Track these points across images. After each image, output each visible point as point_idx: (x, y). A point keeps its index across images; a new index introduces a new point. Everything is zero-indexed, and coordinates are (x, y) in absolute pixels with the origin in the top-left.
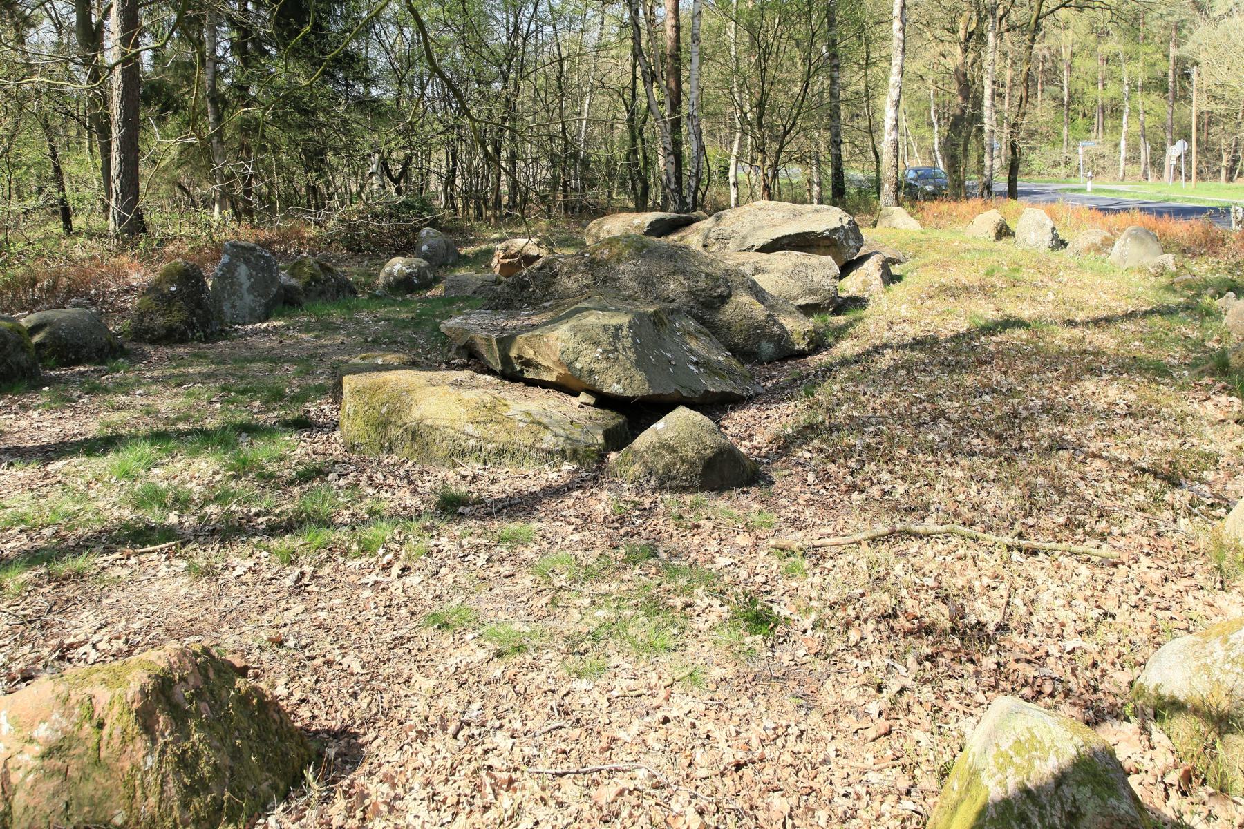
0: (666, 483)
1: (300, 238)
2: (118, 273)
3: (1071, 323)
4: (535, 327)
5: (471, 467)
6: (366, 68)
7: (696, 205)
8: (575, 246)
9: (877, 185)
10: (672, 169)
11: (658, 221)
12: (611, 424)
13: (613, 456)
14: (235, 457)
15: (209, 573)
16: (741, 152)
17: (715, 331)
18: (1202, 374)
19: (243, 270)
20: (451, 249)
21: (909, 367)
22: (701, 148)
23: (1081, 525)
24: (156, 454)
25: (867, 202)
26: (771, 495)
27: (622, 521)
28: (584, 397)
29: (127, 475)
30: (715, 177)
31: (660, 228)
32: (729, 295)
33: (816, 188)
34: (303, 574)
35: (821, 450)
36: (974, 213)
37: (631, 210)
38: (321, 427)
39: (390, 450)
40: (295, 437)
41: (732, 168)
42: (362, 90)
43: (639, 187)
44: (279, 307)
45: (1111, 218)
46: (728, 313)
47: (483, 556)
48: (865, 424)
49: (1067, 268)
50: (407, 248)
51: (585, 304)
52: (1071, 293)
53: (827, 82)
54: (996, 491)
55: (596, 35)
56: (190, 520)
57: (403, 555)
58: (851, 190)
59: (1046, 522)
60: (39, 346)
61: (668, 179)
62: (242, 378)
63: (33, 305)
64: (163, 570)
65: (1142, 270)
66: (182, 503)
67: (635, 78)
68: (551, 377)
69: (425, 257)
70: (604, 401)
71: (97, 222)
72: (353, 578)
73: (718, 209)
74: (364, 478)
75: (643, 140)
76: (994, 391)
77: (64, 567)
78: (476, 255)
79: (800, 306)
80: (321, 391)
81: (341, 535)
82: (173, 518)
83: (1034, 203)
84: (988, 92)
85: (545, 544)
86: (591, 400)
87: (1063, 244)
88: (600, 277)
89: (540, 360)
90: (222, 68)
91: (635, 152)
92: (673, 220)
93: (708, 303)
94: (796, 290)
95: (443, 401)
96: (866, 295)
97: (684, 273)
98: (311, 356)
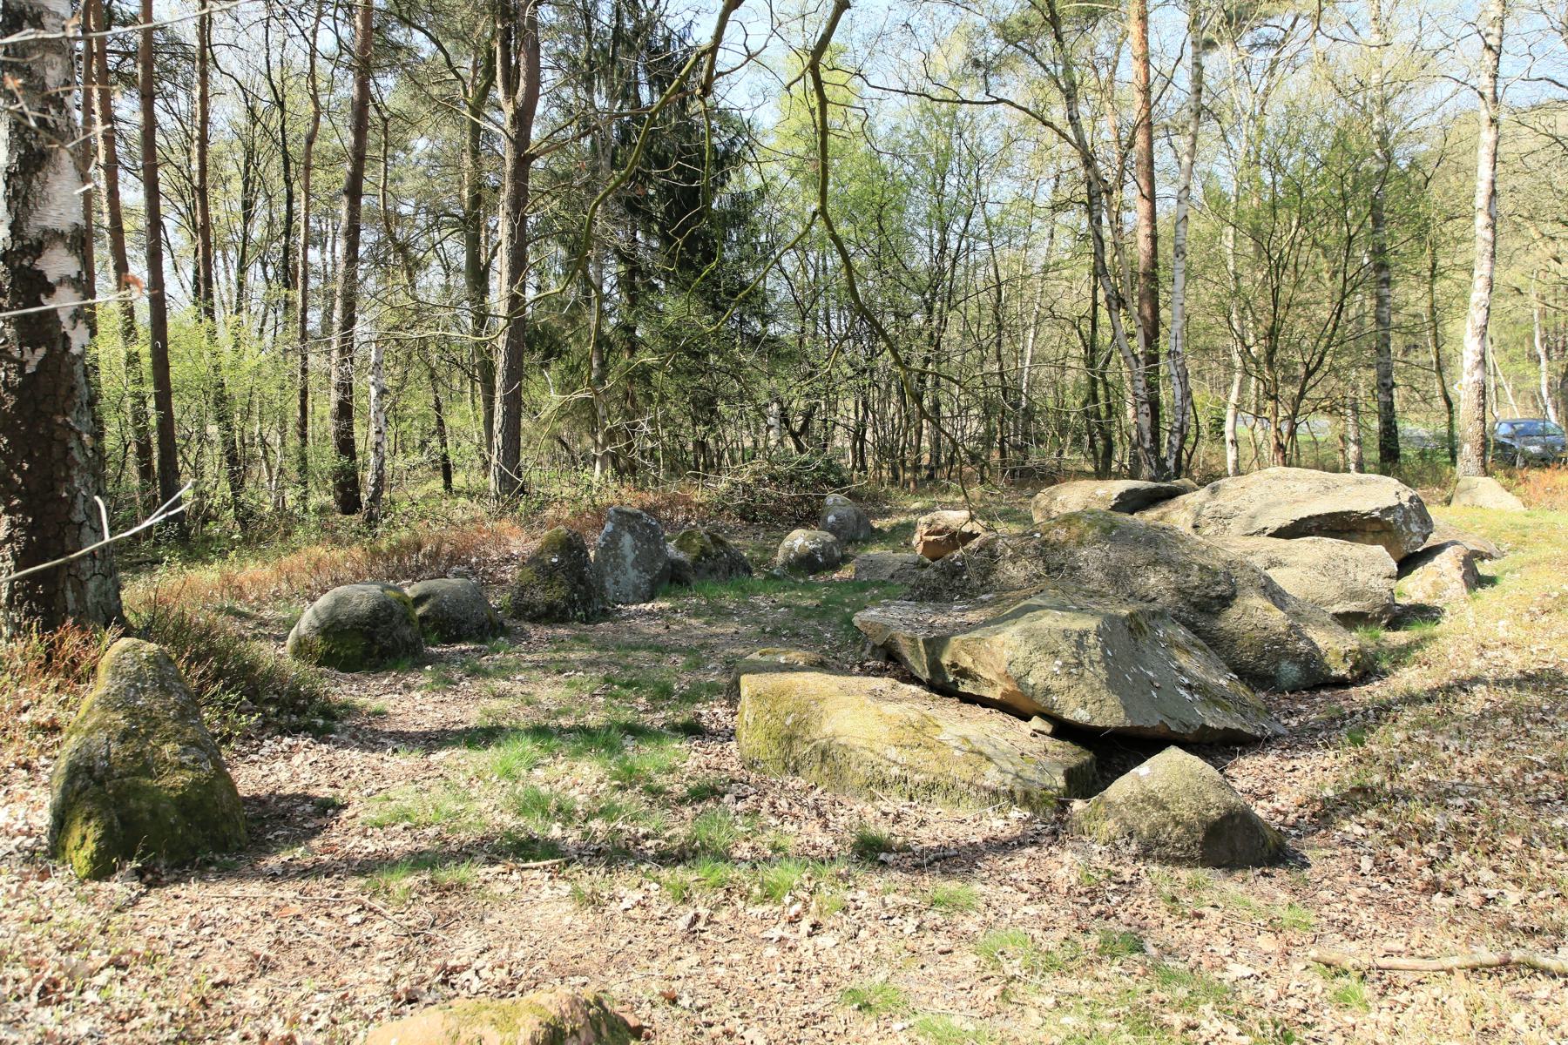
1: (687, 502)
2: (499, 539)
4: (970, 627)
5: (894, 802)
6: (765, 300)
8: (1018, 521)
10: (1146, 422)
11: (1129, 492)
13: (1078, 805)
14: (621, 763)
15: (593, 901)
17: (1215, 643)
20: (862, 520)
22: (1187, 394)
25: (1436, 470)
27: (1093, 895)
28: (1037, 723)
30: (1204, 432)
31: (1133, 502)
32: (1233, 596)
33: (1353, 448)
34: (697, 917)
37: (1087, 475)
38: (714, 735)
39: (796, 772)
40: (685, 745)
41: (1229, 419)
42: (759, 327)
43: (1100, 444)
44: (666, 586)
47: (911, 922)
50: (810, 517)
53: (1370, 303)
55: (1043, 251)
57: (813, 907)
58: (1408, 451)
60: (423, 619)
61: (1141, 435)
62: (626, 668)
63: (416, 573)
64: (547, 893)
66: (565, 813)
67: (1095, 305)
68: (995, 694)
69: (832, 530)
70: (1064, 730)
71: (476, 480)
72: (754, 929)
73: (1210, 478)
74: (765, 804)
75: (1106, 384)
77: (448, 875)
78: (894, 529)
79: (1336, 615)
80: (714, 690)
81: (740, 873)
82: (556, 831)
86: (1048, 728)
88: (1054, 564)
89: (980, 670)
90: (607, 306)
91: (1095, 399)
92: (1150, 491)
95: (861, 715)
98: (702, 646)
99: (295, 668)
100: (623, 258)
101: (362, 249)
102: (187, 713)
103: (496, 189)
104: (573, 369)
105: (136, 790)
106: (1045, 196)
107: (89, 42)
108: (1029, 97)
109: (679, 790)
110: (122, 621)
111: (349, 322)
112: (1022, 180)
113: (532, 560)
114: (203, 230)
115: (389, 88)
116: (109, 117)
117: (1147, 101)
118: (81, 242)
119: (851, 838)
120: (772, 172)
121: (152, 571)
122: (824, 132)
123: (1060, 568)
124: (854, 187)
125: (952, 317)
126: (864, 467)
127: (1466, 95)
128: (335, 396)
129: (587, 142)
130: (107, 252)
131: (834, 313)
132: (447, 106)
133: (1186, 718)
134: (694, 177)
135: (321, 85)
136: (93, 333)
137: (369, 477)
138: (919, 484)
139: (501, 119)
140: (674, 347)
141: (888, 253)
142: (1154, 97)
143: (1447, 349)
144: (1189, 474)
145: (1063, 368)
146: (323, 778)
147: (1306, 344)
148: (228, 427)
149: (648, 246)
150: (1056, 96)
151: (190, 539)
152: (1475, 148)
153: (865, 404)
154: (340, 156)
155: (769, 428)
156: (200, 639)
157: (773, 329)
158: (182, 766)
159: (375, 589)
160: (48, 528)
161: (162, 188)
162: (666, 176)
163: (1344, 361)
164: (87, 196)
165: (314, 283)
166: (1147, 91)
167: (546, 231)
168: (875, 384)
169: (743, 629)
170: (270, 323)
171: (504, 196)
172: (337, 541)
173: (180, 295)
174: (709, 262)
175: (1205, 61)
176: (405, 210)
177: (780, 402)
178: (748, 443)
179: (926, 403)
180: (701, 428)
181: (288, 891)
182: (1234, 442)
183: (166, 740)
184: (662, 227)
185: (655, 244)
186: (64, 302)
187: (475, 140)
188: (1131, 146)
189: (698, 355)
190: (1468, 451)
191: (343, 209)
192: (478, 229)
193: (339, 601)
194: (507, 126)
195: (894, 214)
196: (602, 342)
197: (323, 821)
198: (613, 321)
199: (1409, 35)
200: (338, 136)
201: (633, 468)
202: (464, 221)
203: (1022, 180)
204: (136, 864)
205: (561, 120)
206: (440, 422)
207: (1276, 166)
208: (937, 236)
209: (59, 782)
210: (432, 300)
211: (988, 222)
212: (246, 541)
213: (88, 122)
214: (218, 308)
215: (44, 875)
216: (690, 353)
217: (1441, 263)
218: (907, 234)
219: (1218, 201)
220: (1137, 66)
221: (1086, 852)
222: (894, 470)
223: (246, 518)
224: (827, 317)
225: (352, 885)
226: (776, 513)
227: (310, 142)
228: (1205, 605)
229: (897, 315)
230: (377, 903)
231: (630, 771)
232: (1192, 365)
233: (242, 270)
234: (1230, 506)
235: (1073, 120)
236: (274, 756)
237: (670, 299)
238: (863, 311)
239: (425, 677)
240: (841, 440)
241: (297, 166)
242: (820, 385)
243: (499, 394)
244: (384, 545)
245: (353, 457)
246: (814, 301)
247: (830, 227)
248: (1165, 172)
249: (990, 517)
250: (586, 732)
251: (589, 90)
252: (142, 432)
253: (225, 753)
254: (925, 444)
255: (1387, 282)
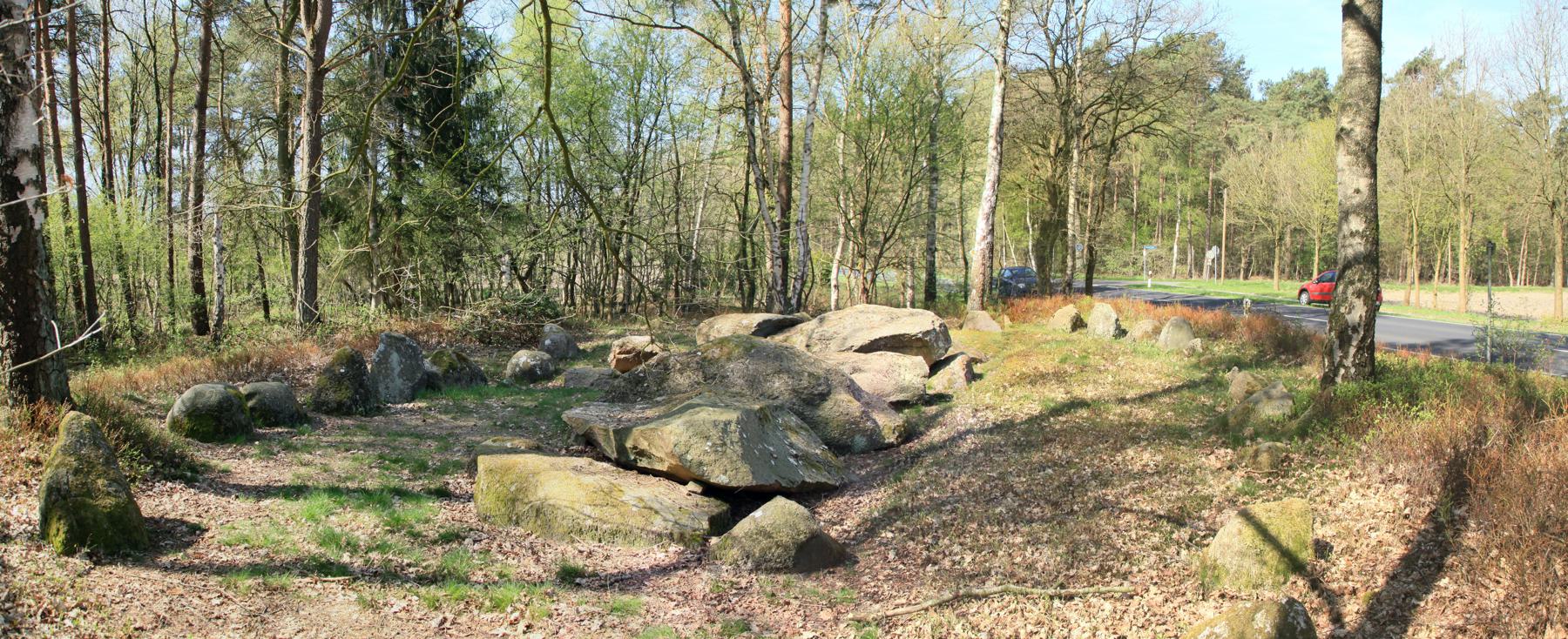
0: (761, 565)
1: (439, 329)
2: (302, 354)
3: (1123, 401)
4: (648, 420)
5: (587, 544)
6: (500, 176)
7: (800, 306)
8: (686, 343)
9: (965, 290)
10: (779, 271)
11: (765, 322)
12: (716, 511)
13: (714, 540)
14: (391, 515)
15: (372, 605)
16: (843, 257)
17: (814, 425)
18: (1210, 434)
19: (395, 357)
20: (571, 344)
21: (986, 449)
22: (808, 252)
23: (1110, 569)
24: (332, 505)
25: (956, 306)
26: (855, 573)
27: (720, 598)
28: (692, 486)
29: (312, 517)
30: (818, 280)
31: (767, 329)
32: (829, 393)
33: (910, 291)
34: (445, 620)
35: (902, 530)
36: (1055, 308)
37: (736, 310)
38: (458, 497)
39: (517, 523)
40: (437, 504)
41: (834, 270)
42: (496, 197)
43: (746, 287)
44: (423, 391)
45: (1160, 310)
46: (828, 409)
47: (597, 622)
48: (943, 504)
49: (1124, 353)
50: (532, 341)
51: (696, 401)
52: (1126, 375)
53: (926, 193)
54: (1047, 551)
55: (712, 143)
56: (358, 562)
57: (527, 614)
58: (941, 294)
59: (1084, 571)
60: (252, 409)
61: (775, 281)
62: (394, 449)
63: (246, 378)
64: (340, 598)
65: (1179, 352)
66: (353, 547)
67: (748, 184)
68: (663, 467)
69: (548, 351)
70: (710, 490)
71: (286, 312)
72: (485, 628)
73: (820, 312)
74: (495, 545)
75: (753, 244)
76: (1055, 464)
77: (275, 580)
78: (594, 350)
79: (892, 403)
80: (458, 466)
81: (475, 592)
82: (346, 558)
83: (1103, 299)
84: (1072, 200)
85: (649, 617)
86: (699, 489)
87: (1124, 333)
88: (710, 373)
89: (653, 451)
90: (380, 182)
91: (744, 254)
92: (779, 321)
93: (810, 400)
94: (889, 389)
95: (565, 483)
96: (950, 392)
97: (788, 372)
98: (450, 435)
99: (171, 437)
100: (393, 145)
101: (207, 147)
102: (110, 461)
103: (299, 97)
104: (355, 230)
105: (84, 506)
106: (714, 101)
107: (38, 22)
108: (705, 25)
109: (433, 535)
110: (70, 400)
111: (199, 199)
112: (697, 89)
113: (327, 370)
114: (107, 141)
115: (224, 26)
116: (51, 72)
117: (789, 36)
118: (37, 156)
119: (556, 568)
120: (508, 77)
121: (85, 369)
122: (549, 45)
123: (714, 377)
124: (571, 89)
125: (642, 189)
126: (573, 304)
127: (988, 59)
128: (191, 253)
129: (366, 57)
130: (52, 161)
131: (553, 186)
132: (265, 37)
133: (792, 477)
134: (448, 81)
135: (180, 30)
136: (46, 215)
137: (214, 309)
138: (615, 316)
139: (303, 44)
140: (431, 212)
141: (596, 140)
142: (794, 34)
143: (968, 227)
144: (806, 309)
145: (723, 231)
146: (192, 511)
147: (886, 219)
148: (125, 275)
149: (411, 134)
150: (725, 26)
151: (105, 350)
152: (991, 95)
153: (575, 256)
154: (192, 80)
155: (502, 273)
156: (114, 414)
157: (506, 198)
158: (109, 494)
159: (220, 387)
160: (28, 342)
161: (82, 115)
162: (426, 80)
163: (907, 233)
164: (40, 125)
165: (176, 173)
166: (789, 29)
167: (335, 126)
168: (583, 241)
169: (480, 423)
170: (149, 203)
171: (305, 101)
172: (195, 353)
173: (94, 187)
174: (458, 146)
175: (829, 11)
176: (236, 116)
177: (510, 254)
178: (486, 285)
179: (621, 255)
180: (450, 274)
181: (175, 579)
182: (836, 287)
183: (99, 477)
184: (422, 120)
185: (417, 133)
186: (30, 196)
187: (285, 60)
188: (777, 68)
189: (449, 218)
190: (974, 294)
191: (194, 120)
192: (287, 127)
193: (198, 395)
194: (308, 48)
195: (601, 110)
196: (377, 209)
197: (194, 538)
198: (384, 193)
199: (957, 14)
200: (191, 66)
201: (399, 304)
202: (276, 121)
203: (697, 89)
204: (87, 550)
205: (347, 41)
206: (261, 270)
207: (873, 94)
208: (634, 128)
209: (42, 495)
210: (255, 181)
211: (672, 119)
212: (139, 352)
213: (40, 76)
214: (117, 195)
215: (39, 549)
216: (442, 216)
217: (968, 170)
218: (611, 126)
219: (834, 114)
220: (783, 10)
221: (717, 571)
222: (596, 305)
223: (138, 336)
224: (549, 189)
225: (214, 580)
226: (506, 337)
227: (172, 73)
228: (810, 399)
229: (601, 188)
230: (230, 594)
231: (398, 520)
232: (811, 232)
233: (131, 167)
234: (832, 331)
235: (737, 46)
236: (162, 493)
237: (428, 176)
238: (576, 185)
239: (255, 449)
240: (557, 283)
241: (165, 90)
242: (542, 241)
243: (302, 249)
244: (225, 357)
245: (204, 295)
246: (539, 176)
247: (552, 118)
248: (800, 90)
249: (665, 341)
250: (365, 491)
251: (369, 17)
252: (75, 279)
253: (133, 489)
254: (620, 287)
255: (936, 180)
